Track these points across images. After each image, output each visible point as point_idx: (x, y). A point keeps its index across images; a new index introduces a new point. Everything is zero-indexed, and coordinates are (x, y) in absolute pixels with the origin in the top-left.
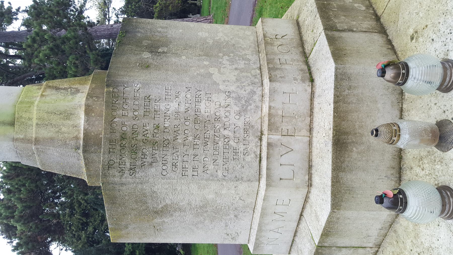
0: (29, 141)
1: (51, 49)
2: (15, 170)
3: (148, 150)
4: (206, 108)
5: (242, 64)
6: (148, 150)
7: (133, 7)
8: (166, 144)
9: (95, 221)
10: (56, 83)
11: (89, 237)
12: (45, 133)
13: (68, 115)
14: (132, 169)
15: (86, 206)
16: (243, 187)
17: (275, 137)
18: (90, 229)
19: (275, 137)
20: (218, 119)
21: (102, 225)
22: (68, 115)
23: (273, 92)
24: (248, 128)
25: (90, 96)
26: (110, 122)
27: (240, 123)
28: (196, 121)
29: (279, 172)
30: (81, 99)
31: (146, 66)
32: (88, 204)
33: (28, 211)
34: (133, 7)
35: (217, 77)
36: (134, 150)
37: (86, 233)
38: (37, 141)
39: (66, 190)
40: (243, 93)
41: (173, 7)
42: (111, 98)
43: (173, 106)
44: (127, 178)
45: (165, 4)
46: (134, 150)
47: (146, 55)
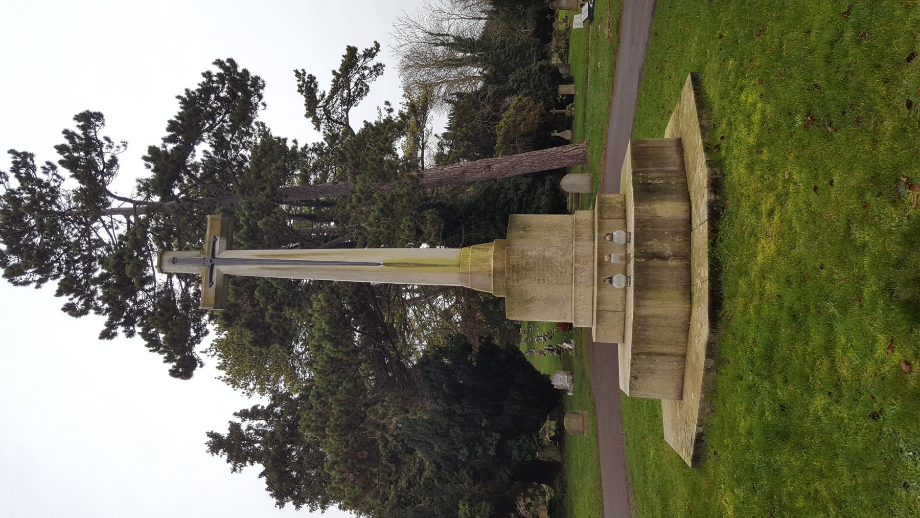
0: (467, 273)
1: (382, 210)
2: (332, 362)
3: (524, 272)
4: (547, 254)
5: (564, 234)
6: (524, 272)
7: (464, 130)
8: (531, 269)
9: (409, 470)
10: (477, 246)
11: (400, 497)
12: (475, 269)
13: (485, 260)
14: (517, 280)
15: (395, 446)
16: (565, 287)
17: (578, 265)
18: (403, 483)
19: (578, 265)
20: (553, 258)
21: (420, 477)
22: (485, 260)
23: (576, 246)
24: (566, 262)
25: (495, 251)
26: (508, 261)
27: (563, 260)
28: (543, 259)
29: (579, 280)
30: (491, 253)
31: (522, 237)
32: (398, 442)
33: (345, 419)
34: (464, 130)
35: (552, 240)
36: (518, 272)
37: (396, 487)
38: (471, 273)
39: (378, 406)
40: (564, 247)
41: (526, 125)
42: (507, 249)
43: (534, 253)
44: (516, 284)
45: (514, 122)
46: (518, 272)
47: (521, 232)
